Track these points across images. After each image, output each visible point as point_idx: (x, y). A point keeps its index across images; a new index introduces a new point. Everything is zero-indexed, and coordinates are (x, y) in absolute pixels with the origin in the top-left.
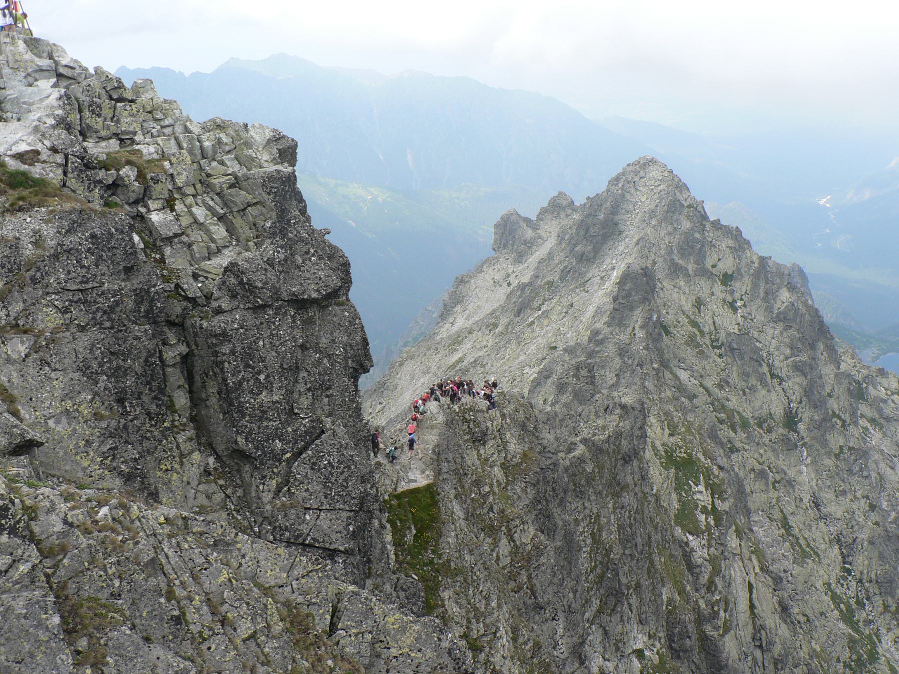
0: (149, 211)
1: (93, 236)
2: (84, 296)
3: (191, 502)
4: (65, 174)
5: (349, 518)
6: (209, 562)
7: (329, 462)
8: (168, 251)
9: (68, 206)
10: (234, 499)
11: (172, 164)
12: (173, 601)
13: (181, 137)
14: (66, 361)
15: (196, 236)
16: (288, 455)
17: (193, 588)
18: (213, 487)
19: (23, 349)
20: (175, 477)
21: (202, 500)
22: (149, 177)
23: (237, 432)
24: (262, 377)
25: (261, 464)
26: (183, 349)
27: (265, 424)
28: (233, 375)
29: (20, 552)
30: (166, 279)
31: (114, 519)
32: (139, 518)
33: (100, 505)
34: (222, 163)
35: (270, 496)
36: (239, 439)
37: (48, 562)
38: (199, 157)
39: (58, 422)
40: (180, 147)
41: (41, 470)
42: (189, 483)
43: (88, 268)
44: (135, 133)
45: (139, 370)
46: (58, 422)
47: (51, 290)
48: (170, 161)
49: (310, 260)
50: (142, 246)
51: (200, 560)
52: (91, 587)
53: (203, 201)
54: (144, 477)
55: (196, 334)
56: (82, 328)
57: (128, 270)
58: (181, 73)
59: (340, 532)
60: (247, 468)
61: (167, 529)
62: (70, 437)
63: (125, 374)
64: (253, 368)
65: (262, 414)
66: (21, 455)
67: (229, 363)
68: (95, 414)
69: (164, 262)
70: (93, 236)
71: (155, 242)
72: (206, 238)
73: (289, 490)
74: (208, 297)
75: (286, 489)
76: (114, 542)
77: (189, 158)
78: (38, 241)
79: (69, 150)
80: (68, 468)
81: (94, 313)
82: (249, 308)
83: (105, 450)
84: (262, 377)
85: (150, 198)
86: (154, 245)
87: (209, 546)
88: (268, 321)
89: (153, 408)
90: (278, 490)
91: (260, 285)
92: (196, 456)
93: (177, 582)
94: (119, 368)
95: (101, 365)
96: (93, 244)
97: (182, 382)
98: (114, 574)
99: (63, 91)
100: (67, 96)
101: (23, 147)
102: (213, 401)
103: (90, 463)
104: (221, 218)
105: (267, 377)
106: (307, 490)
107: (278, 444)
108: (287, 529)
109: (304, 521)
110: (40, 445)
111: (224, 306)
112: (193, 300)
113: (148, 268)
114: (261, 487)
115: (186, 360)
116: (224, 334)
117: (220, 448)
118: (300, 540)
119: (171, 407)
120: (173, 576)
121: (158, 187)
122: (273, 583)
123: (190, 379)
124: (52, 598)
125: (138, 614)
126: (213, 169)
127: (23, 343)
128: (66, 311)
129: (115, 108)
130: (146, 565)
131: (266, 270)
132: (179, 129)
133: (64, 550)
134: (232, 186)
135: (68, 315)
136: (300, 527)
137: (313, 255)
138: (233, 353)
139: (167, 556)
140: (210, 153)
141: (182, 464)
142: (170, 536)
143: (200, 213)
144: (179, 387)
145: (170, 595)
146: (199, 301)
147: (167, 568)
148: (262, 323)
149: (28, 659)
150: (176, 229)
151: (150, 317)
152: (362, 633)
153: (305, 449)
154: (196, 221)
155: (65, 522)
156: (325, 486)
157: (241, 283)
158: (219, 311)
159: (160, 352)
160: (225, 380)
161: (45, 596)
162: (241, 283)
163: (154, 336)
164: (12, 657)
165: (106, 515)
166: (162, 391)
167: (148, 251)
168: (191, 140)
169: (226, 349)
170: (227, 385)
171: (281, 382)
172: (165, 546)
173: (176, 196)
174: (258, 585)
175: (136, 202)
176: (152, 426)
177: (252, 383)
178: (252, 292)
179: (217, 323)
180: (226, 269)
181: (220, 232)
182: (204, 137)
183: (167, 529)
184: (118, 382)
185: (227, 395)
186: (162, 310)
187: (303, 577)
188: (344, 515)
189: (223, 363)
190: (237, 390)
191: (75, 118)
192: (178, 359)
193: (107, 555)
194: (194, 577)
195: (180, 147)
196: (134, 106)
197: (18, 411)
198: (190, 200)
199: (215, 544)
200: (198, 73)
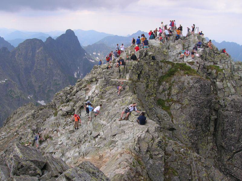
0: (217, 81)
1: (201, 85)
2: (195, 99)
4: (199, 69)
6: (202, 170)
8: (219, 92)
9: (197, 77)
10: (217, 157)
11: (225, 71)
12: (191, 176)
13: (229, 65)
14: (187, 112)
15: (227, 90)
16: (234, 151)
17: (196, 174)
18: (213, 153)
19: (178, 107)
21: (209, 155)
22: (218, 73)
23: (223, 141)
24: (233, 130)
25: (227, 151)
26: (216, 117)
27: (231, 141)
28: (226, 127)
29: (161, 152)
30: (216, 99)
31: (184, 152)
33: (182, 148)
34: (238, 73)
35: (227, 160)
36: (223, 143)
37: (166, 156)
39: (181, 126)
40: (228, 67)
41: (174, 135)
42: (207, 150)
43: (198, 92)
44: (218, 62)
45: (203, 119)
46: (181, 126)
47: (188, 95)
48: (225, 70)
50: (213, 89)
51: (200, 169)
52: (174, 165)
53: (231, 82)
54: (197, 144)
55: (220, 114)
56: (193, 106)
57: (207, 95)
58: (239, 45)
60: (223, 151)
61: (195, 159)
62: (183, 130)
63: (200, 119)
64: (232, 127)
65: (231, 139)
66: (171, 131)
67: (226, 124)
68: (190, 127)
69: (217, 94)
70: (201, 85)
71: (216, 89)
72: (229, 91)
73: (232, 160)
74: (225, 106)
75: (231, 159)
76: (181, 157)
77: (230, 70)
78: (188, 83)
79: (201, 64)
80: (180, 137)
81: (196, 103)
82: (235, 111)
83: (190, 135)
84: (233, 130)
85: (218, 78)
86: (216, 90)
87: (204, 166)
88: (239, 116)
89: (204, 129)
90: (229, 159)
91: (239, 106)
92: (211, 144)
93: (193, 172)
94: (199, 117)
95: (195, 115)
96: (200, 87)
97: (213, 125)
98: (179, 164)
100: (204, 50)
101: (191, 61)
102: (220, 132)
103: (185, 137)
104: (234, 87)
105: (235, 130)
106: (237, 162)
108: (228, 170)
109: (233, 169)
110: (176, 130)
112: (221, 106)
113: (213, 95)
114: (225, 157)
115: (216, 120)
116: (227, 116)
117: (218, 144)
118: (231, 174)
119: (209, 130)
120: (193, 170)
121: (220, 76)
123: (216, 125)
124: (164, 164)
125: (181, 175)
126: (236, 74)
127: (179, 106)
128: (190, 101)
129: (214, 55)
130: (187, 165)
132: (229, 62)
133: (170, 155)
134: (239, 79)
135: (190, 102)
136: (232, 171)
138: (228, 121)
139: (193, 165)
140: (236, 70)
142: (195, 161)
143: (229, 85)
144: (212, 126)
145: (191, 174)
146: (223, 106)
147: (192, 167)
148: (237, 116)
149: (155, 175)
150: (222, 87)
151: (210, 107)
153: (239, 151)
154: (227, 86)
155: (173, 149)
157: (235, 105)
158: (227, 110)
159: (210, 116)
160: (224, 128)
161: (163, 163)
162: (235, 105)
163: (209, 112)
164: (152, 173)
165: (182, 151)
166: (208, 126)
167: (214, 91)
168: (231, 66)
169: (226, 120)
170: (224, 129)
171: (238, 132)
172: (194, 162)
173: (224, 79)
175: (214, 79)
176: (203, 133)
177: (230, 130)
179: (226, 113)
180: (232, 100)
181: (233, 90)
182: (235, 66)
183: (195, 159)
184: (197, 121)
185: (224, 132)
186: (213, 106)
189: (224, 123)
191: (204, 56)
192: (214, 119)
193: (179, 160)
194: (198, 172)
195: (228, 67)
196: (219, 55)
197: (173, 121)
198: (227, 81)
199: (206, 166)
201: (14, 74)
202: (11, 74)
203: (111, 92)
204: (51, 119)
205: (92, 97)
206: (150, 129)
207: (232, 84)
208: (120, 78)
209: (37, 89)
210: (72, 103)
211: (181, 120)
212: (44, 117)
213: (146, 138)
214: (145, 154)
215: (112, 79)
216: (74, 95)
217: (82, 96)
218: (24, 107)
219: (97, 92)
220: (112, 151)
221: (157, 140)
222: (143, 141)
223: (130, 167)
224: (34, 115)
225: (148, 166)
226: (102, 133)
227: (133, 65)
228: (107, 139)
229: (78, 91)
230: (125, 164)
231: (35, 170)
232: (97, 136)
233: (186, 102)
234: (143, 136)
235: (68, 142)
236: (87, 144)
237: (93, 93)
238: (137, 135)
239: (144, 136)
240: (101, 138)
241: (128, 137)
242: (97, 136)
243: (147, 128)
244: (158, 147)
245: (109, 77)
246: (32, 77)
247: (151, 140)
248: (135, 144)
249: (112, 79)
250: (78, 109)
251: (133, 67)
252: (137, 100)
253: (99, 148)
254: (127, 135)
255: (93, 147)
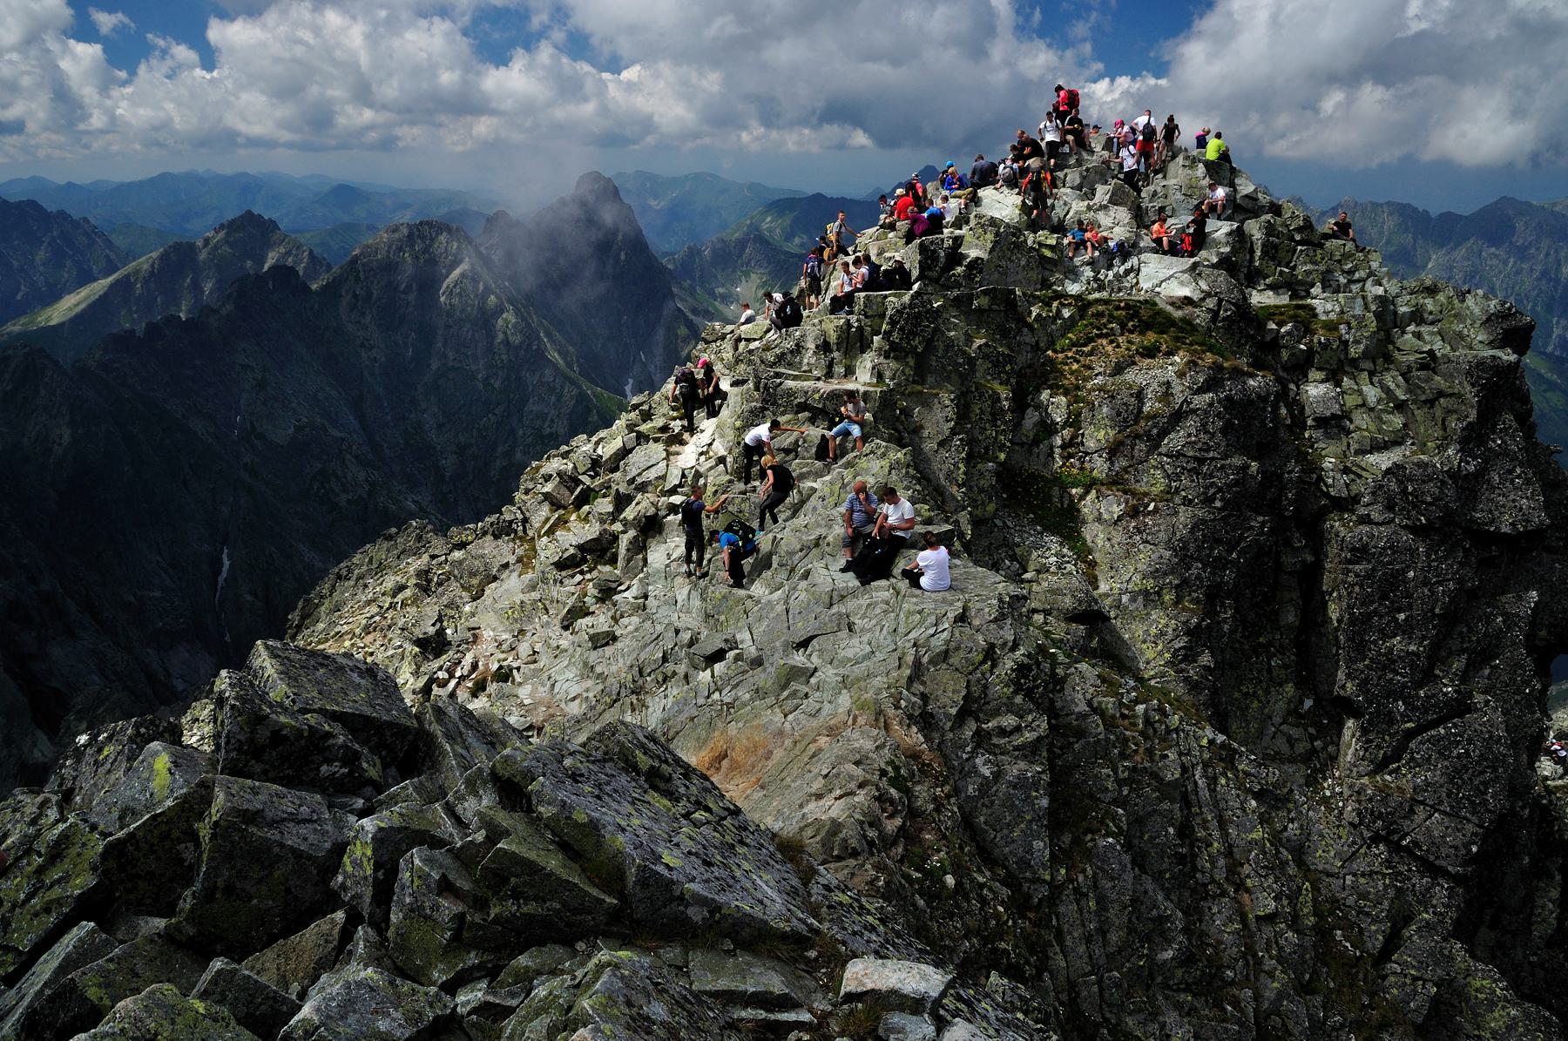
3: (1266, 741)
5: (1475, 834)
7: (1467, 751)
18: (1295, 732)
20: (1255, 704)
24: (1402, 616)
29: (1030, 718)
32: (1177, 730)
38: (1390, 325)
43: (1213, 435)
44: (1313, 285)
49: (1512, 482)
56: (1187, 502)
59: (1456, 848)
95: (1199, 549)
99: (1236, 225)
107: (1401, 706)
111: (1375, 516)
122: (1320, 867)
131: (1443, 482)
134: (1423, 367)
137: (1519, 477)
141: (1267, 692)
152: (1425, 981)
156: (1451, 781)
157: (1404, 492)
174: (1300, 863)
178: (1415, 506)
180: (1388, 471)
187: (1363, 875)
188: (1470, 828)
190: (1363, 623)
200: (1450, 214)
201: (334, 393)
202: (320, 396)
203: (785, 445)
204: (505, 586)
205: (698, 475)
206: (974, 606)
207: (1387, 391)
208: (829, 375)
209: (449, 463)
210: (604, 505)
211: (1118, 555)
212: (475, 581)
213: (958, 648)
214: (952, 729)
215: (790, 384)
216: (616, 469)
217: (653, 470)
218: (385, 545)
219: (720, 449)
220: (790, 717)
221: (1008, 664)
222: (944, 666)
223: (878, 789)
224: (427, 572)
225: (970, 788)
226: (744, 636)
227: (889, 313)
228: (766, 664)
229: (631, 451)
230: (851, 777)
231: (351, 759)
232: (718, 656)
233: (1153, 481)
234: (938, 643)
235: (587, 690)
236: (675, 690)
237: (701, 454)
238: (912, 635)
239: (948, 642)
240: (738, 658)
241: (868, 649)
242: (718, 656)
243: (960, 604)
244: (1016, 692)
245: (778, 375)
246: (424, 405)
247: (983, 662)
248: (904, 682)
249: (790, 384)
250: (632, 533)
251: (893, 323)
252: (913, 477)
253: (730, 706)
254: (865, 639)
255: (701, 701)
